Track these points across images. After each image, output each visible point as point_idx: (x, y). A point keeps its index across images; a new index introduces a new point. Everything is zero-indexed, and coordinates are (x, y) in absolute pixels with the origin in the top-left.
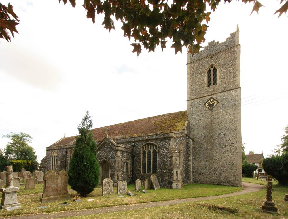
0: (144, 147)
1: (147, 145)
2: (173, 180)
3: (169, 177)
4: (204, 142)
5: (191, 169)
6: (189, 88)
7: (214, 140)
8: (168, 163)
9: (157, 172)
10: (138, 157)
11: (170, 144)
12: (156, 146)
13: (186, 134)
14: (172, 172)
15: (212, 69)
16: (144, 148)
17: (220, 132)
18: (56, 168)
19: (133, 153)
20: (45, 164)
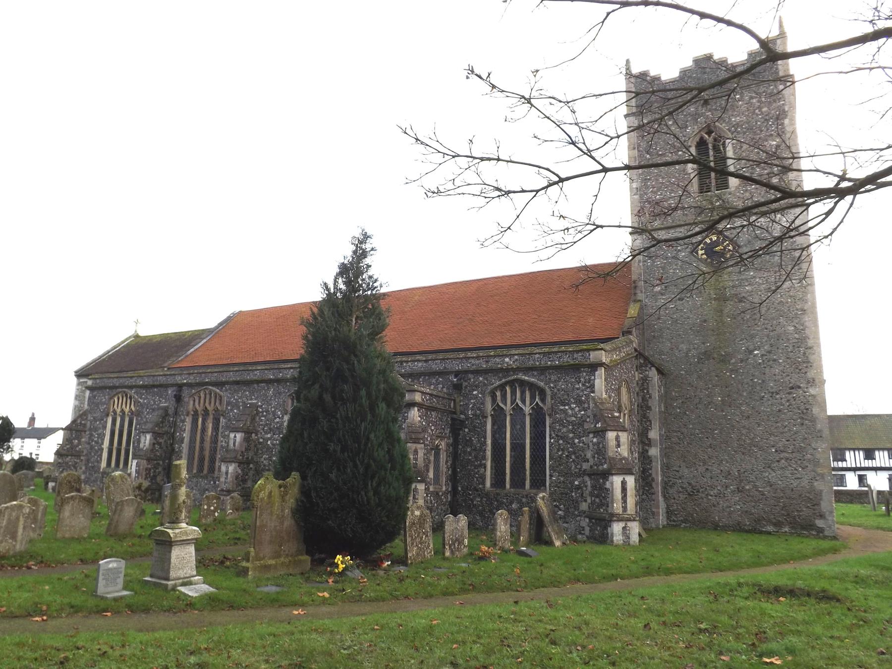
0: (498, 394)
1: (508, 389)
2: (612, 515)
3: (593, 503)
4: (699, 377)
5: (657, 474)
6: (635, 191)
7: (732, 371)
8: (589, 455)
9: (548, 484)
10: (475, 427)
11: (592, 388)
12: (542, 393)
13: (636, 350)
14: (608, 485)
15: (710, 140)
16: (499, 398)
17: (751, 347)
18: (135, 462)
19: (455, 413)
20: (79, 443)
